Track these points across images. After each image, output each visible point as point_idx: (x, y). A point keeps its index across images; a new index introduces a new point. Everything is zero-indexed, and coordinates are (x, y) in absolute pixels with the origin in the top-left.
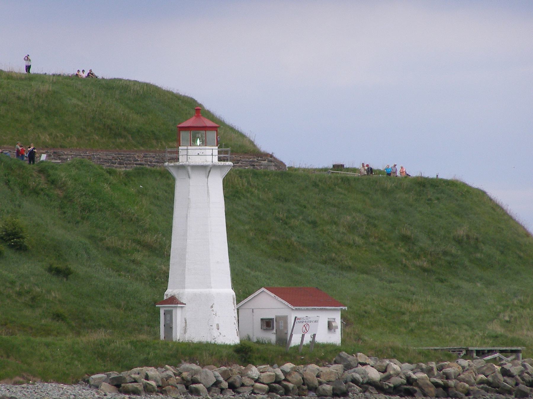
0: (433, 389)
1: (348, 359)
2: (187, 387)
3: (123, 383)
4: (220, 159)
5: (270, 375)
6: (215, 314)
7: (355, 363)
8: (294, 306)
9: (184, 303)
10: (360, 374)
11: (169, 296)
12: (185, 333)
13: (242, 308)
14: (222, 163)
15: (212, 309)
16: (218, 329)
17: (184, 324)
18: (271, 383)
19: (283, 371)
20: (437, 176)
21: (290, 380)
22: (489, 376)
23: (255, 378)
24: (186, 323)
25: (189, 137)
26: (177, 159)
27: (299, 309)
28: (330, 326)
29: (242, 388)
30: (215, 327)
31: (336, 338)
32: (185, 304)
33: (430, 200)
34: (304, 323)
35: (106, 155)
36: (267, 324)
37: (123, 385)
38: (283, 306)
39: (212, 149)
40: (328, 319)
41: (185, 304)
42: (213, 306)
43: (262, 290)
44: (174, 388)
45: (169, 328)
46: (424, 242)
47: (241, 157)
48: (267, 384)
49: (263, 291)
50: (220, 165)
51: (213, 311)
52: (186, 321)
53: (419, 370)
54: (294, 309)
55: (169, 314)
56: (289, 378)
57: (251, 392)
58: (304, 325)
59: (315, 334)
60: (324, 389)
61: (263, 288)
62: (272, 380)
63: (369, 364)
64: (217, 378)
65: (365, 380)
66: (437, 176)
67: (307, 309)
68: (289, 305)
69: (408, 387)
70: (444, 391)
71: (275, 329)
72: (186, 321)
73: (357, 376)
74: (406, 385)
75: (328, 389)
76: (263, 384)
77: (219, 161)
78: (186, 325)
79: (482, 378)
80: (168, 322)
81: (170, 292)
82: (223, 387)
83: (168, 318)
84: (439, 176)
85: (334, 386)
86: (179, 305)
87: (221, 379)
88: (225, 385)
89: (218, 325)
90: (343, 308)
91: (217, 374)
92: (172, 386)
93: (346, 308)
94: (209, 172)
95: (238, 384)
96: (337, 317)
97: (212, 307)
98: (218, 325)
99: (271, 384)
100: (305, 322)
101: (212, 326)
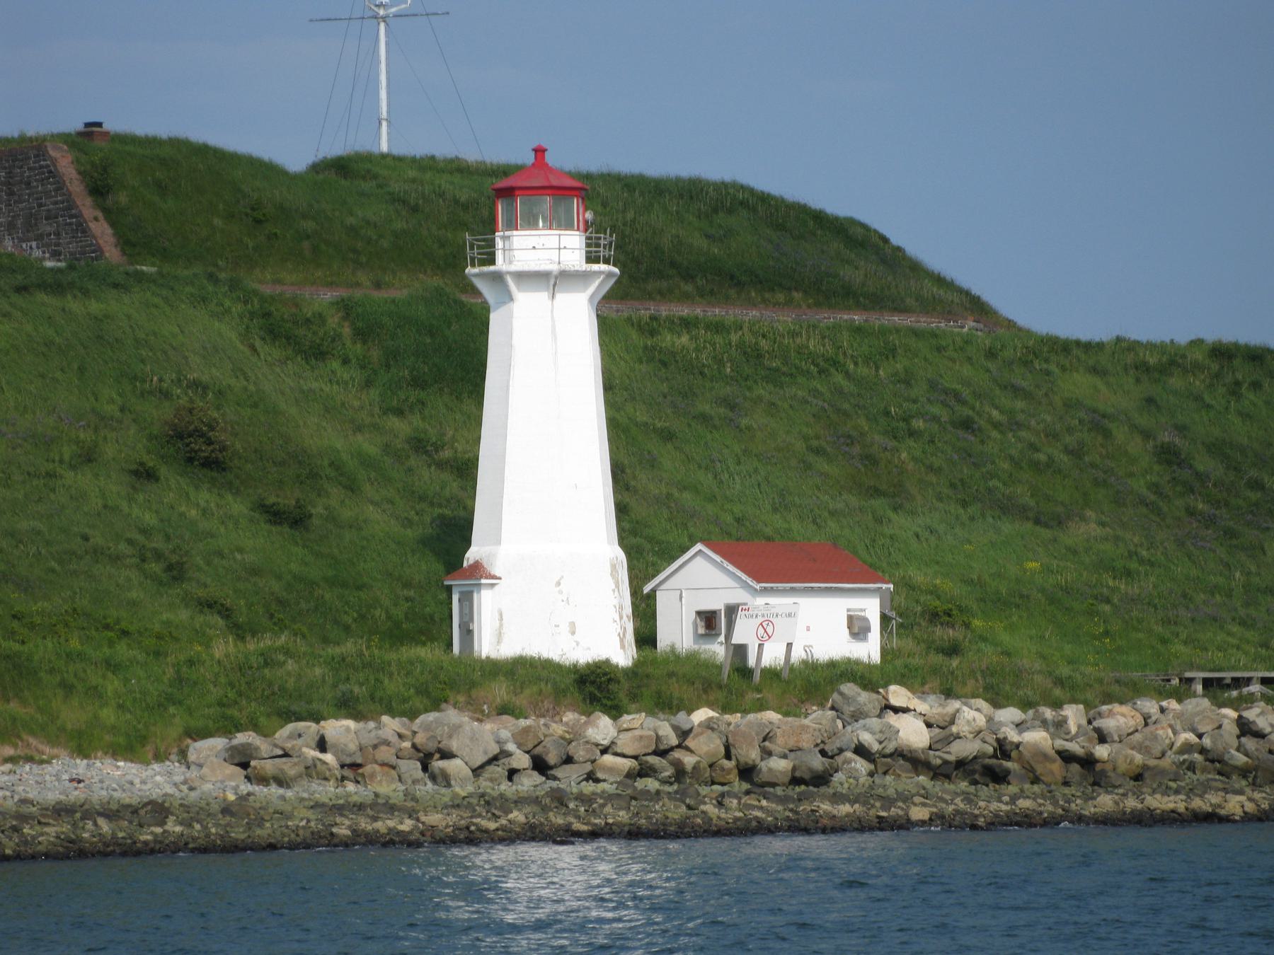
0: (1057, 767)
1: (859, 699)
2: (425, 768)
3: (255, 759)
4: (591, 259)
5: (641, 737)
6: (565, 599)
7: (874, 709)
8: (759, 581)
9: (498, 575)
10: (873, 733)
11: (471, 562)
12: (499, 642)
13: (662, 587)
14: (595, 267)
15: (558, 589)
16: (573, 633)
17: (498, 622)
18: (644, 755)
19: (675, 728)
20: (540, 152)
21: (693, 749)
22: (1205, 736)
23: (602, 742)
24: (501, 619)
25: (514, 216)
26: (491, 260)
27: (772, 588)
28: (857, 628)
29: (568, 767)
30: (565, 628)
31: (870, 650)
32: (500, 578)
33: (1238, 384)
34: (760, 620)
35: (618, 311)
36: (708, 620)
37: (253, 763)
38: (731, 583)
39: (560, 235)
40: (848, 610)
41: (500, 578)
42: (561, 582)
43: (698, 549)
44: (386, 769)
45: (467, 633)
46: (1205, 463)
47: (913, 319)
48: (635, 757)
49: (700, 550)
50: (577, 271)
51: (561, 592)
52: (501, 615)
53: (1037, 723)
54: (758, 588)
55: (467, 598)
56: (690, 743)
57: (585, 776)
58: (761, 624)
59: (791, 644)
60: (770, 770)
61: (699, 544)
62: (647, 748)
63: (915, 710)
64: (1123, 738)
65: (890, 748)
66: (540, 152)
67: (793, 589)
68: (749, 581)
69: (994, 761)
70: (1083, 771)
71: (723, 635)
72: (501, 615)
73: (867, 738)
74: (990, 757)
75: (780, 769)
76: (624, 756)
77: (587, 262)
78: (501, 625)
79: (1186, 739)
80: (466, 619)
81: (472, 555)
82: (515, 764)
83: (466, 611)
84: (550, 159)
85: (797, 762)
86: (483, 581)
87: (511, 747)
88: (521, 760)
89: (572, 625)
90: (884, 586)
91: (505, 734)
92: (383, 764)
93: (891, 586)
94: (554, 285)
95: (552, 759)
96: (871, 608)
97: (558, 584)
98: (572, 625)
99: (644, 758)
100: (763, 616)
101: (558, 626)
